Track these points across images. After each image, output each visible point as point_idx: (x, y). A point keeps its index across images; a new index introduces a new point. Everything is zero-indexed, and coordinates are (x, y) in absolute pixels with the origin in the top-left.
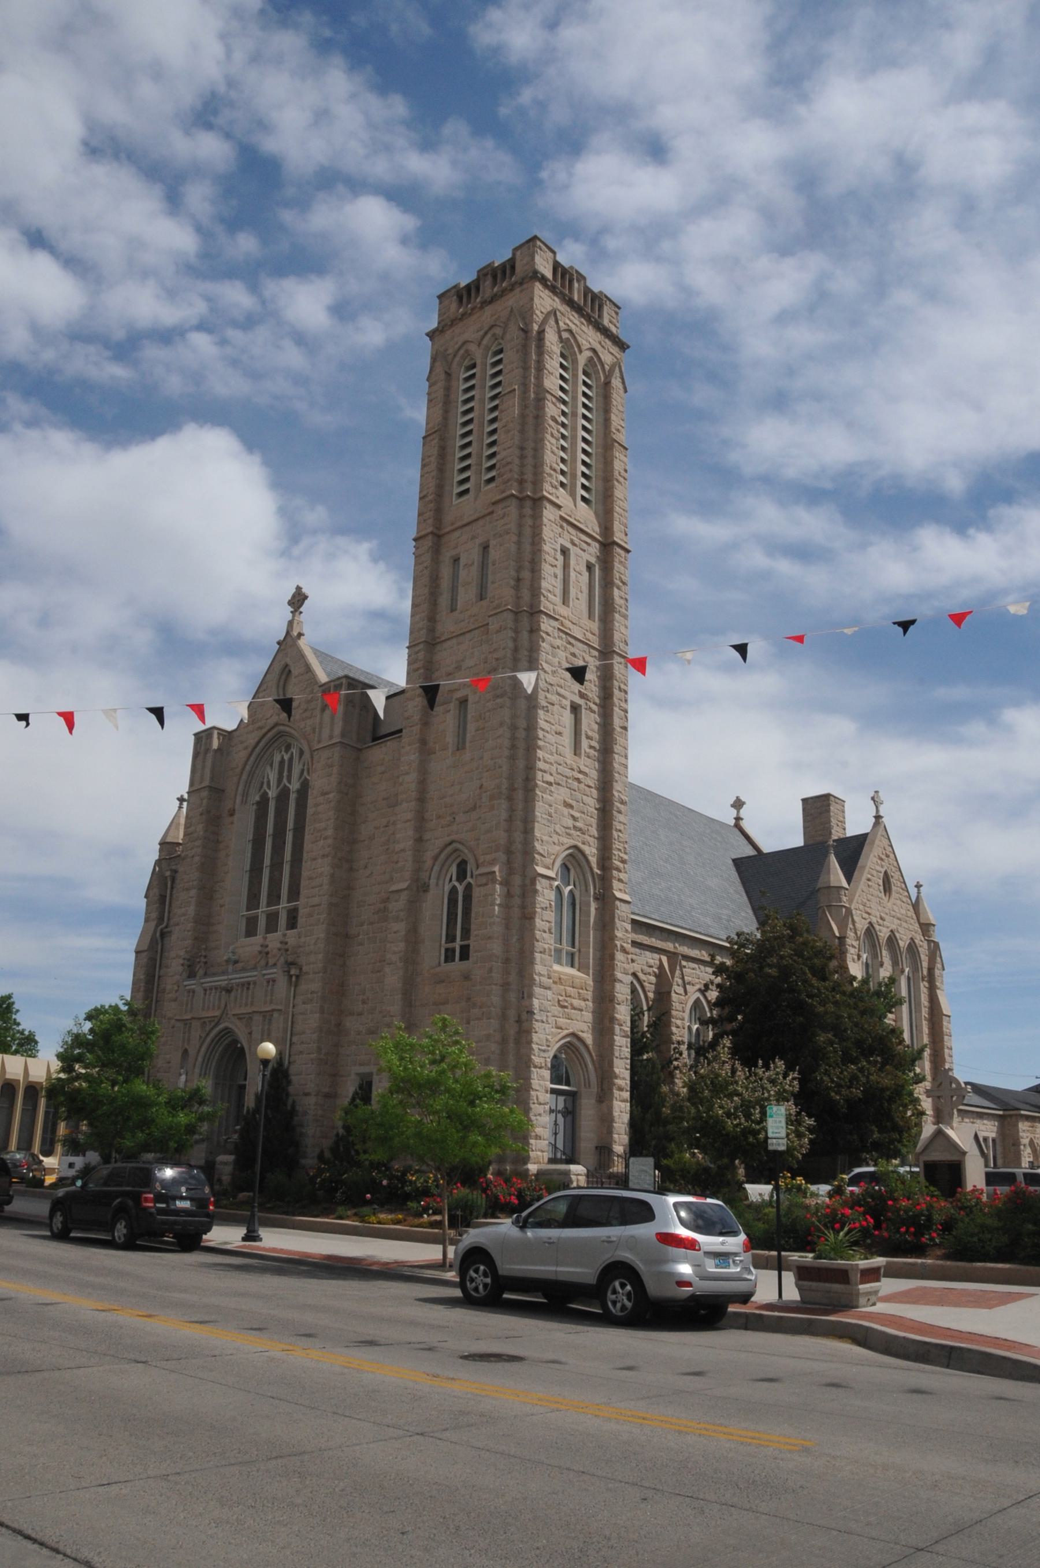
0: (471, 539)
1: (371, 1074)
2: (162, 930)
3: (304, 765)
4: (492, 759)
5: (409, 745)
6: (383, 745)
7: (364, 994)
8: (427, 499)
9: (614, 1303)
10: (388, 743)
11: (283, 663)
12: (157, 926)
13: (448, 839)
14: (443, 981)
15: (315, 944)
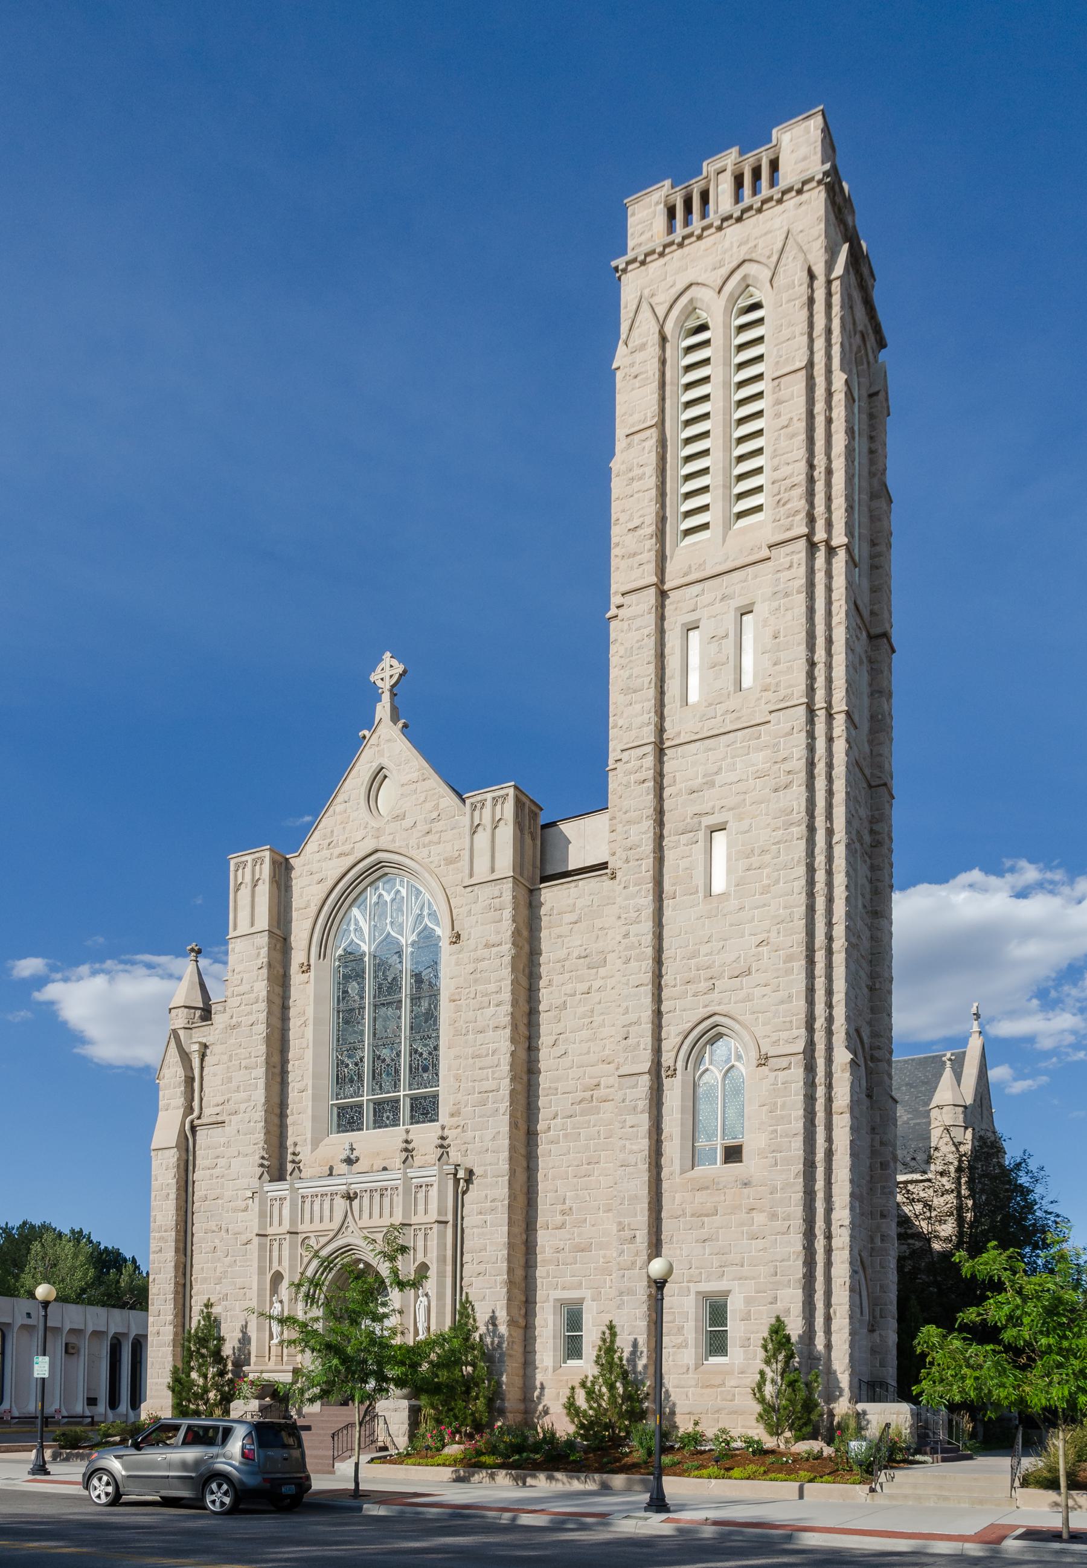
0: (722, 599)
1: (580, 1302)
2: (192, 1121)
3: (422, 909)
4: (785, 908)
5: (635, 885)
6: (573, 884)
7: (564, 1203)
8: (640, 532)
9: (213, 1502)
10: (581, 883)
11: (375, 766)
12: (185, 1116)
13: (703, 1012)
14: (707, 1188)
15: (494, 1139)
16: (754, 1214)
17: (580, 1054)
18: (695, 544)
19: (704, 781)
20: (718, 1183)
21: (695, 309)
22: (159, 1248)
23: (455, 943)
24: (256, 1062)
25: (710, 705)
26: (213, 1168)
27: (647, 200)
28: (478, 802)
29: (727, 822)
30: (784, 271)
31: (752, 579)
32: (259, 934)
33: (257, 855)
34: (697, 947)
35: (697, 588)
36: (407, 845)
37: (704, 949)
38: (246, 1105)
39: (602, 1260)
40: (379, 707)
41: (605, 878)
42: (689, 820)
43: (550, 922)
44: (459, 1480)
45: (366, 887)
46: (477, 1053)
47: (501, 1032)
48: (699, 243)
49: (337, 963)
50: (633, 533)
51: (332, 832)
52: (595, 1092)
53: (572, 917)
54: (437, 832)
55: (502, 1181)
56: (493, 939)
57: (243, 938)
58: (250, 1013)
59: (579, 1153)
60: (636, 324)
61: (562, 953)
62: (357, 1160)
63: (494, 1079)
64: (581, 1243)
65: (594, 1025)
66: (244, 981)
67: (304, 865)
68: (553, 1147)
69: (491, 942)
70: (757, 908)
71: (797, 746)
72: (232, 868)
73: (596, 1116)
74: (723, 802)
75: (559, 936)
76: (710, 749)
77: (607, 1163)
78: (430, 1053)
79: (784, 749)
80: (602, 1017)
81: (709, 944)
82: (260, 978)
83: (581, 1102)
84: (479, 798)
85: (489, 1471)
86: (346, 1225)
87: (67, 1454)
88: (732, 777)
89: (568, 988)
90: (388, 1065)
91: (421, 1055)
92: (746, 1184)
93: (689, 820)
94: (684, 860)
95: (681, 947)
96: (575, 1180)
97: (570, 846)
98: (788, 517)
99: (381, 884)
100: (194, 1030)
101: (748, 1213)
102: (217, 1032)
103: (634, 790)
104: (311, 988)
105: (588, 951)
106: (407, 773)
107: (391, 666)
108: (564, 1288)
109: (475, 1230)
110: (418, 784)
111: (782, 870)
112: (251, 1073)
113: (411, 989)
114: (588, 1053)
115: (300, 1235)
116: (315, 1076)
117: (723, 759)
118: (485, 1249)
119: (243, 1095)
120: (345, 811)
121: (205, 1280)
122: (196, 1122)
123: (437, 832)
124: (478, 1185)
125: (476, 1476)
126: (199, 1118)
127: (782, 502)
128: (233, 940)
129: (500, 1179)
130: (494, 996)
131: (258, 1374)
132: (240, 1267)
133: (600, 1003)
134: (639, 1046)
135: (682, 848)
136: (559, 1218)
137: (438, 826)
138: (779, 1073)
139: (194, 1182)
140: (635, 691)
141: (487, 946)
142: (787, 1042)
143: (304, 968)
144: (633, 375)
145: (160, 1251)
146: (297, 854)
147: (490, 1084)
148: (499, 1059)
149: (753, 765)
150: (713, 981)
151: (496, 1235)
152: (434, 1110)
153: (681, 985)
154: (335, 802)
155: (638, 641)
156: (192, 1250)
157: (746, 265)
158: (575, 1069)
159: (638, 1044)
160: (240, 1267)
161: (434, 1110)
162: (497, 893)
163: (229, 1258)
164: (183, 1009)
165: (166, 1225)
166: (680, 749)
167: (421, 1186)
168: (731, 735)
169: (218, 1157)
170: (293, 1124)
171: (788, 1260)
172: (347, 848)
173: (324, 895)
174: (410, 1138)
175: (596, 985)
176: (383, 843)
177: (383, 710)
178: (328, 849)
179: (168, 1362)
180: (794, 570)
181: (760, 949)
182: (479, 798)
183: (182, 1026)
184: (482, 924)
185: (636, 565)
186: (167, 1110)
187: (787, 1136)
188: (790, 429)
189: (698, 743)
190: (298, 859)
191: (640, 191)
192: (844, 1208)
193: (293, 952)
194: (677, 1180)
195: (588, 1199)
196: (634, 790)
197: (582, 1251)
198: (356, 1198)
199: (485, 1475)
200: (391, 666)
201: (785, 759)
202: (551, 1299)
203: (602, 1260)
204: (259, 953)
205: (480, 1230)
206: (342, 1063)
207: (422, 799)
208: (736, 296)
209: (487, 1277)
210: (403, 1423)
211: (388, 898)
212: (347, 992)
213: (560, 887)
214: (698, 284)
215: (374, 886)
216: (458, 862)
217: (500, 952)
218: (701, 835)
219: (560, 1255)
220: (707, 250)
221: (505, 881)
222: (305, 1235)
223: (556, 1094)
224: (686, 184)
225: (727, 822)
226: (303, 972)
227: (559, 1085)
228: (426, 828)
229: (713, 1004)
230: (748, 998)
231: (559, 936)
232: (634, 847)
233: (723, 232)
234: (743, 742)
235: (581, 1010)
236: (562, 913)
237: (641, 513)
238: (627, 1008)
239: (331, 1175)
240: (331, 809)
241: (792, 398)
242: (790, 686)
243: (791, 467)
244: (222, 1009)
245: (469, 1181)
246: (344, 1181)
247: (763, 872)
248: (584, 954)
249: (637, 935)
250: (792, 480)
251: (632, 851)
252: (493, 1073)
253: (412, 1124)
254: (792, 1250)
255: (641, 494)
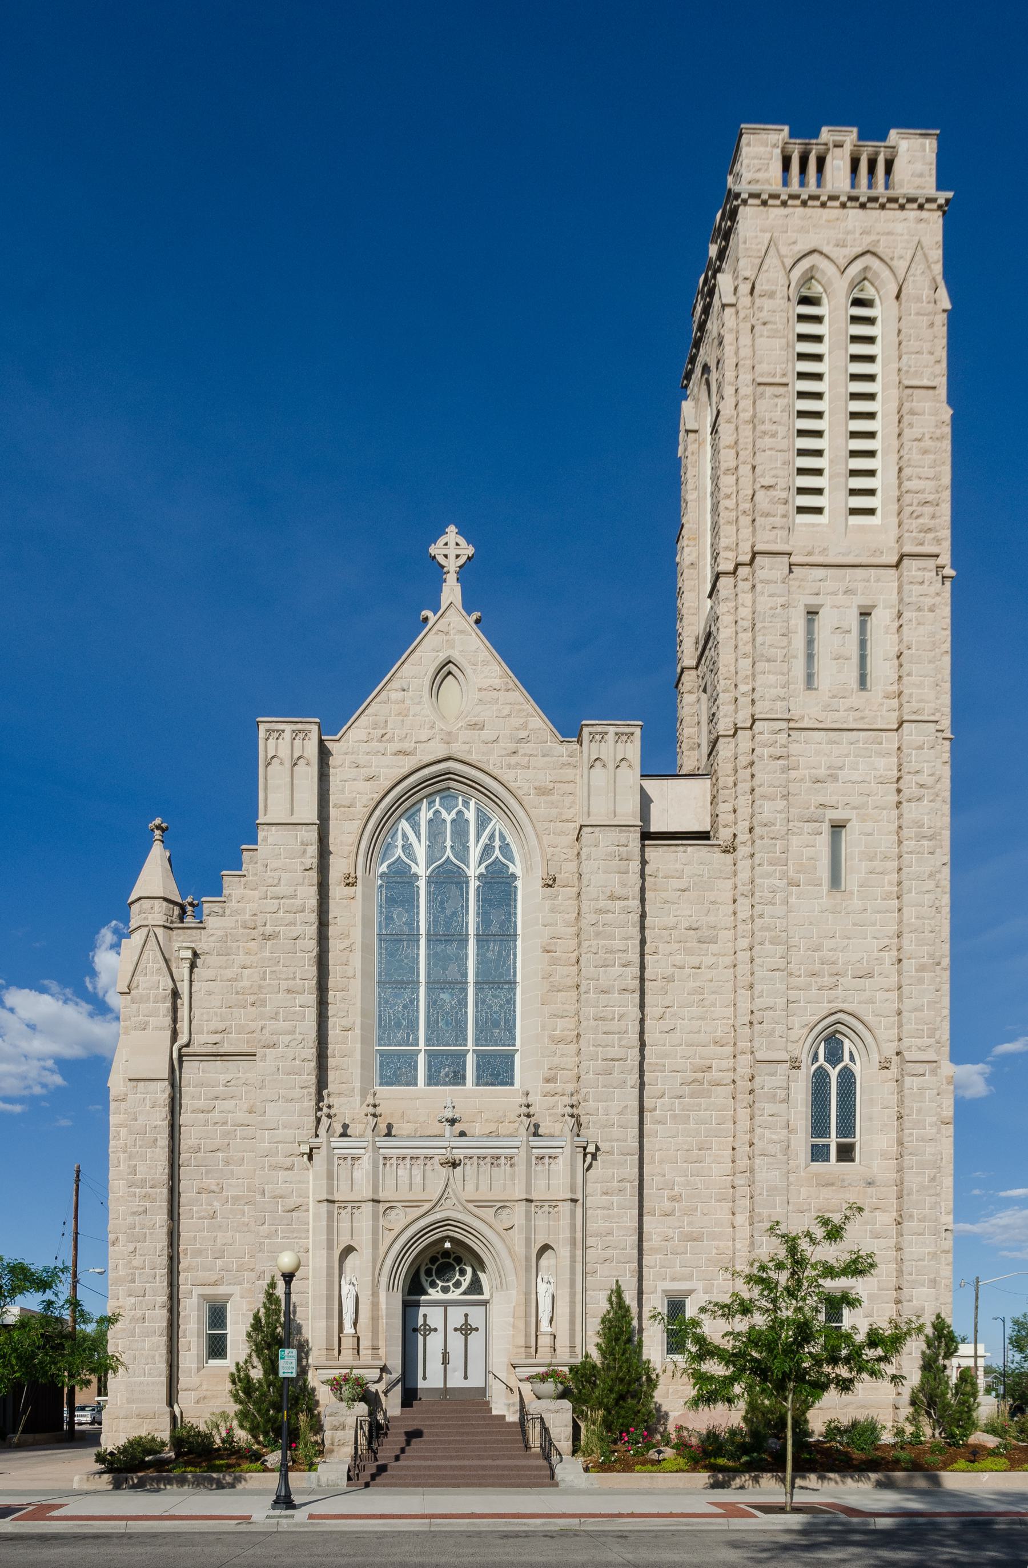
0: (845, 592)
4: (917, 918)
6: (681, 849)
10: (690, 849)
11: (442, 657)
14: (832, 1184)
15: (620, 1113)
16: (877, 1213)
17: (691, 1032)
18: (813, 525)
19: (829, 772)
20: (843, 1181)
21: (812, 278)
22: (143, 1208)
23: (550, 886)
24: (304, 985)
25: (834, 697)
26: (209, 1112)
27: (763, 136)
28: (597, 733)
29: (850, 820)
30: (914, 281)
31: (875, 582)
32: (304, 827)
33: (299, 726)
34: (821, 940)
35: (820, 572)
36: (488, 760)
37: (829, 943)
38: (289, 1037)
39: (714, 1251)
40: (446, 588)
41: (716, 849)
42: (812, 809)
43: (655, 884)
44: (716, 1485)
45: (422, 800)
46: (602, 1015)
47: (628, 996)
48: (820, 210)
49: (380, 882)
50: (766, 491)
51: (386, 721)
52: (706, 1074)
53: (676, 884)
54: (525, 755)
55: (632, 1160)
56: (619, 891)
57: (279, 827)
58: (294, 924)
59: (690, 1136)
60: (765, 267)
61: (670, 921)
62: (335, 1115)
63: (620, 1046)
64: (692, 1232)
65: (706, 1003)
66: (282, 882)
67: (346, 754)
68: (659, 1127)
69: (616, 894)
70: (879, 912)
71: (928, 762)
72: (262, 734)
73: (707, 1100)
74: (847, 799)
75: (666, 902)
76: (835, 742)
77: (720, 1150)
78: (501, 1006)
79: (916, 762)
80: (714, 996)
81: (833, 940)
82: (306, 881)
83: (692, 1082)
84: (599, 729)
85: (753, 1475)
86: (445, 1196)
87: (140, 1479)
88: (856, 776)
89: (678, 959)
90: (447, 1013)
91: (490, 1007)
92: (870, 1184)
93: (812, 809)
94: (808, 848)
95: (806, 938)
96: (685, 1165)
97: (652, 805)
98: (920, 532)
99: (438, 800)
100: (175, 932)
101: (872, 1212)
102: (212, 938)
103: (768, 764)
104: (357, 906)
105: (699, 923)
106: (485, 677)
107: (457, 544)
108: (673, 1279)
109: (599, 1211)
110: (500, 693)
111: (914, 880)
112: (295, 998)
113: (478, 928)
114: (699, 1032)
115: (381, 1204)
116: (365, 1014)
117: (847, 756)
118: (612, 1233)
119: (282, 1025)
120: (403, 701)
121: (198, 1253)
122: (185, 1050)
123: (525, 755)
124: (603, 1162)
125: (738, 1480)
126: (187, 1045)
127: (915, 515)
128: (266, 827)
129: (629, 1157)
130: (620, 954)
131: (348, 1371)
132: (283, 1238)
133: (711, 981)
134: (774, 1032)
135: (806, 836)
136: (667, 1205)
137: (524, 748)
138: (914, 1078)
139: (180, 1126)
140: (768, 661)
141: (612, 897)
142: (920, 1049)
143: (351, 880)
144: (761, 320)
145: (145, 1212)
146: (337, 737)
147: (615, 1052)
148: (627, 1025)
149: (875, 769)
150: (837, 977)
151: (625, 1219)
152: (507, 1072)
153: (805, 977)
154: (388, 687)
155: (771, 608)
156: (179, 1214)
157: (816, 256)
158: (684, 1047)
159: (773, 1031)
160: (283, 1238)
161: (507, 1072)
162: (623, 841)
163: (266, 1226)
164: (161, 901)
165: (153, 1179)
166: (804, 733)
167: (345, 1159)
168: (854, 733)
169: (217, 1098)
170: (336, 1068)
171: (923, 1260)
172: (407, 746)
173: (377, 797)
174: (377, 1102)
175: (709, 960)
176: (457, 749)
177: (451, 591)
178: (381, 741)
179: (161, 1356)
180: (925, 586)
181: (882, 953)
182: (599, 729)
183: (161, 923)
184: (605, 872)
185: (769, 527)
186: (144, 1029)
187: (923, 1140)
188: (922, 444)
189: (822, 733)
190: (337, 744)
191: (760, 122)
192: (948, 1213)
193: (331, 857)
194: (802, 1174)
195: (700, 1186)
196: (768, 764)
197: (694, 1240)
198: (459, 1165)
199: (747, 1477)
200: (457, 544)
201: (918, 772)
202: (659, 1289)
203: (714, 1251)
204: (305, 851)
205: (605, 1212)
206: (386, 1002)
207: (506, 712)
208: (856, 282)
209: (614, 1264)
210: (566, 1426)
211: (448, 817)
212: (392, 918)
213: (665, 848)
214: (821, 253)
215: (431, 799)
216: (552, 794)
217: (628, 907)
218: (826, 828)
219: (669, 1244)
220: (829, 221)
221: (631, 829)
222: (388, 1205)
223: (664, 1071)
224: (807, 141)
225: (850, 820)
226: (348, 884)
227: (667, 1062)
228: (512, 747)
229: (838, 1000)
230: (871, 1001)
231: (666, 902)
232: (769, 824)
233: (845, 211)
234: (866, 743)
235: (691, 985)
236: (668, 877)
237: (773, 472)
238: (762, 991)
239: (388, 1134)
240: (384, 694)
241: (923, 414)
242: (921, 701)
243: (922, 482)
244: (221, 910)
245: (594, 1156)
246: (446, 1144)
247: (884, 879)
248: (695, 926)
249: (772, 917)
250: (924, 496)
251: (766, 828)
252: (620, 1040)
253: (381, 1084)
254: (927, 1251)
255: (773, 453)
